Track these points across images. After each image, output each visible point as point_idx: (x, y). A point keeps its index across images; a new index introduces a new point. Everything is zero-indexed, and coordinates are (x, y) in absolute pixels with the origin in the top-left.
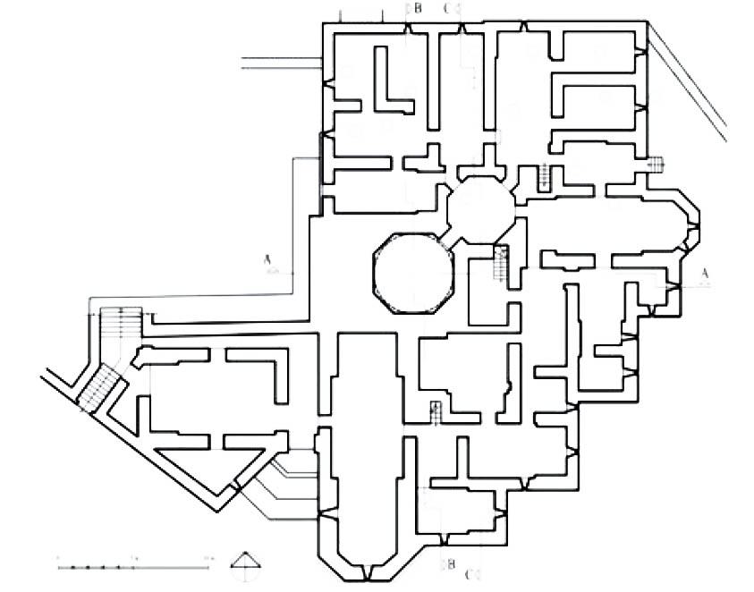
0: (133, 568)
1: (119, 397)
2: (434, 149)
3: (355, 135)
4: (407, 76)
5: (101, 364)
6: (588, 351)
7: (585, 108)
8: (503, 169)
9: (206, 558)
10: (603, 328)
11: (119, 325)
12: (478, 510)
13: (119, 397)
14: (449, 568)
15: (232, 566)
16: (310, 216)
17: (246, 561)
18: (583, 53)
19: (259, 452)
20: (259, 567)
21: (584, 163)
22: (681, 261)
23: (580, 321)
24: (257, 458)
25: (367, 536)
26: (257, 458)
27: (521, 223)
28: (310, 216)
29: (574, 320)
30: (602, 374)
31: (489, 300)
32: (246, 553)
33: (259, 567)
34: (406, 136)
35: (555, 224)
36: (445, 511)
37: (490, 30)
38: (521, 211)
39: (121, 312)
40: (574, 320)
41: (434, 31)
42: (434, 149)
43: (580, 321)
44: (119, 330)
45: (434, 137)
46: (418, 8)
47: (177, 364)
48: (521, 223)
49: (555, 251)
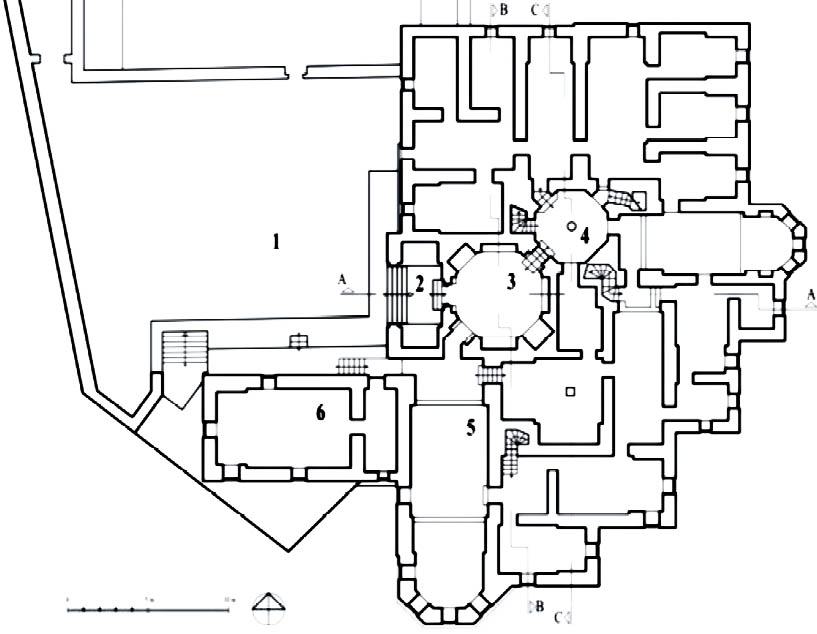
0: (148, 610)
1: (112, 416)
2: (522, 162)
3: (436, 145)
4: (492, 87)
5: (163, 395)
6: (686, 377)
7: (683, 116)
8: (461, 118)
9: (227, 600)
10: (703, 349)
11: (183, 344)
12: (569, 550)
13: (112, 416)
14: (538, 610)
15: (254, 609)
16: (388, 234)
17: (268, 603)
18: (684, 56)
19: (354, 484)
20: (283, 609)
21: (682, 176)
22: (585, 191)
23: (677, 346)
24: (347, 494)
25: (449, 576)
26: (347, 494)
27: (613, 240)
28: (388, 234)
29: (671, 345)
30: (709, 403)
31: (580, 320)
32: (269, 594)
33: (283, 609)
34: (491, 146)
35: (652, 243)
36: (527, 550)
37: (580, 34)
38: (614, 227)
39: (185, 336)
40: (671, 345)
41: (521, 35)
42: (522, 162)
43: (677, 346)
44: (187, 355)
45: (521, 148)
46: (504, 9)
47: (246, 391)
48: (613, 240)
49: (662, 270)
